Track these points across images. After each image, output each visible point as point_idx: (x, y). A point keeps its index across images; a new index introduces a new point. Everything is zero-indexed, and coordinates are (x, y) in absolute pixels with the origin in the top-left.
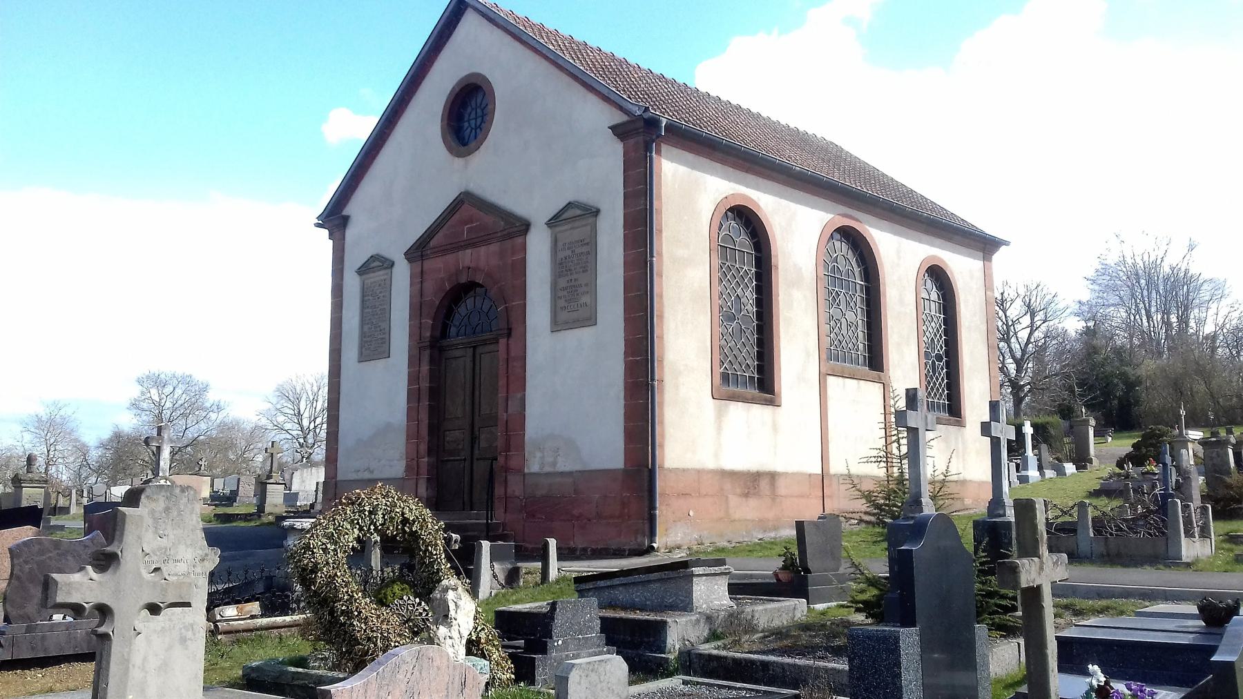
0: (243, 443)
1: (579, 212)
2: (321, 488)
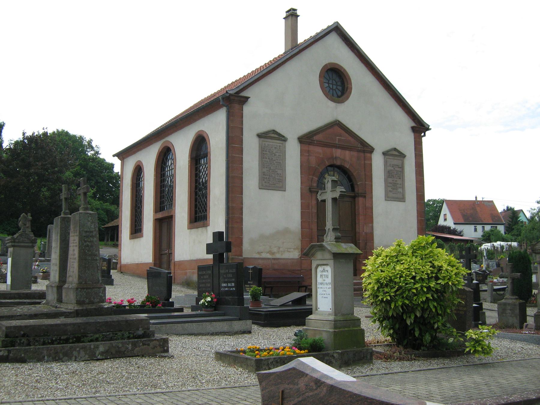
0: (444, 257)
1: (397, 153)
2: (173, 281)
